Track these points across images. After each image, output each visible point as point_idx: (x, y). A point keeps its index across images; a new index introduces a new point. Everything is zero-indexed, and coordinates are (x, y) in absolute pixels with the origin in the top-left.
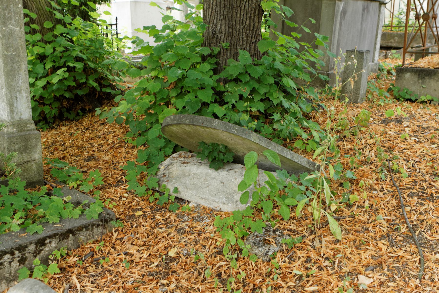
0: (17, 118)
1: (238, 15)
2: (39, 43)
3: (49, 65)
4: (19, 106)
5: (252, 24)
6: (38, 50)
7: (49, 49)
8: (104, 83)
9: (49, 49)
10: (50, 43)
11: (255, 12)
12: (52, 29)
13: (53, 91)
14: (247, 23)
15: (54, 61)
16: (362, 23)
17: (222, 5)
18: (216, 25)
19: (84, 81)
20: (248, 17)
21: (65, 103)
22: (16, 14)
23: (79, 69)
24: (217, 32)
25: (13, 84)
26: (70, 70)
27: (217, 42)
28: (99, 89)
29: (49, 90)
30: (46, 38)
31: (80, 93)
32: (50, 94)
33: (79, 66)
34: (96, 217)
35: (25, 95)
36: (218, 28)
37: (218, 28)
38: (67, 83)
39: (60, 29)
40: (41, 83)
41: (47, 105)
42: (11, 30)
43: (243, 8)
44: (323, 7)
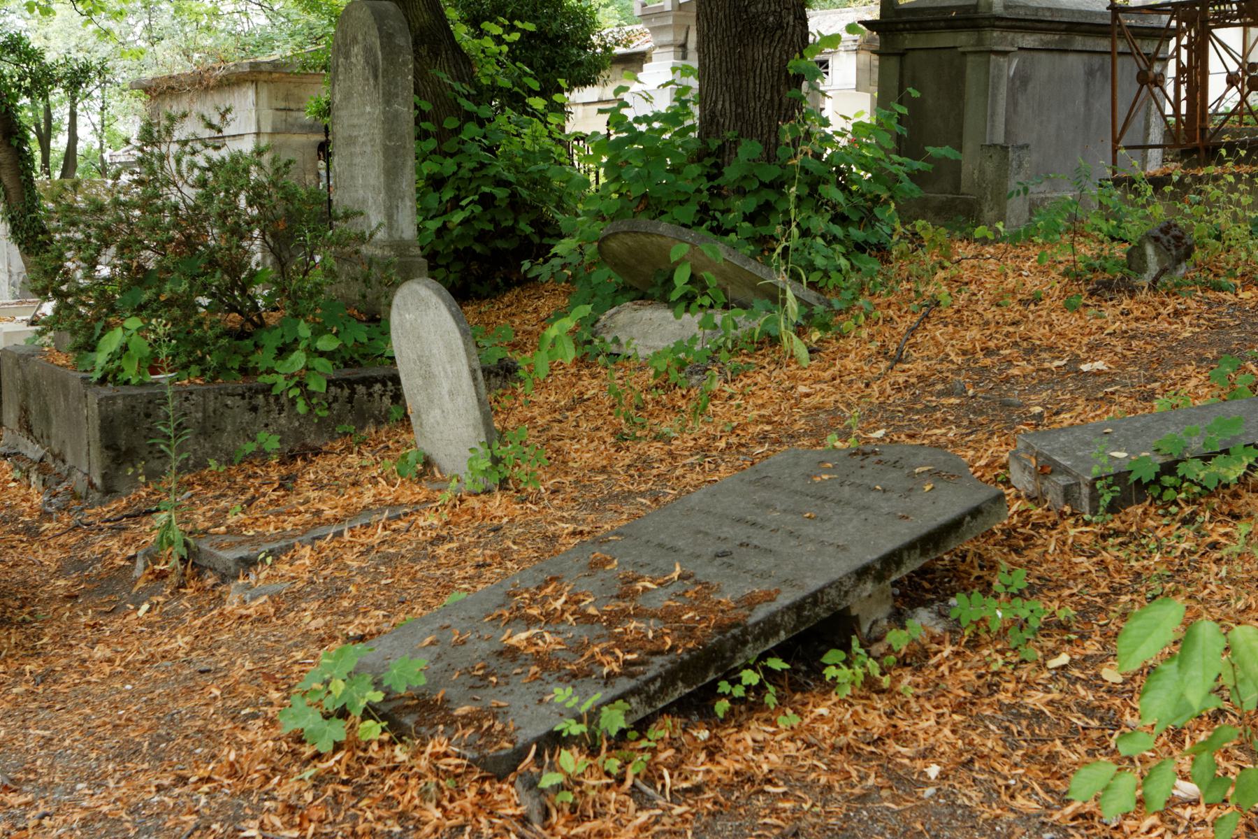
0: (396, 237)
1: (751, 85)
2: (433, 157)
3: (448, 194)
4: (400, 218)
5: (776, 98)
6: (429, 167)
7: (449, 166)
8: (547, 230)
9: (449, 166)
10: (452, 155)
11: (779, 79)
12: (457, 131)
13: (452, 241)
14: (768, 97)
15: (458, 189)
16: (1087, 102)
17: (724, 69)
18: (716, 103)
19: (510, 223)
20: (768, 86)
21: (474, 266)
22: (404, 89)
23: (502, 200)
24: (718, 114)
25: (395, 186)
26: (487, 201)
27: (717, 131)
28: (536, 239)
29: (447, 239)
30: (446, 147)
31: (501, 244)
32: (448, 246)
33: (501, 193)
34: (495, 362)
35: (409, 204)
36: (720, 107)
37: (720, 107)
38: (478, 225)
39: (471, 129)
40: (433, 225)
41: (441, 266)
42: (397, 111)
43: (758, 72)
44: (969, 71)
